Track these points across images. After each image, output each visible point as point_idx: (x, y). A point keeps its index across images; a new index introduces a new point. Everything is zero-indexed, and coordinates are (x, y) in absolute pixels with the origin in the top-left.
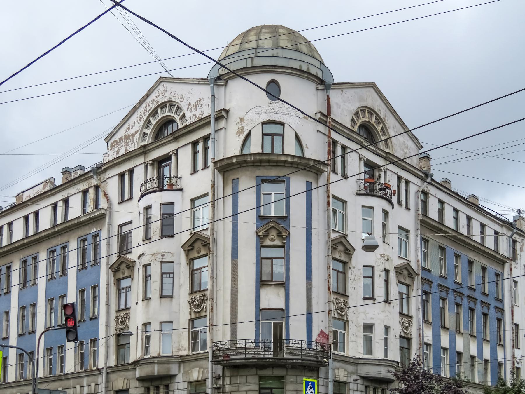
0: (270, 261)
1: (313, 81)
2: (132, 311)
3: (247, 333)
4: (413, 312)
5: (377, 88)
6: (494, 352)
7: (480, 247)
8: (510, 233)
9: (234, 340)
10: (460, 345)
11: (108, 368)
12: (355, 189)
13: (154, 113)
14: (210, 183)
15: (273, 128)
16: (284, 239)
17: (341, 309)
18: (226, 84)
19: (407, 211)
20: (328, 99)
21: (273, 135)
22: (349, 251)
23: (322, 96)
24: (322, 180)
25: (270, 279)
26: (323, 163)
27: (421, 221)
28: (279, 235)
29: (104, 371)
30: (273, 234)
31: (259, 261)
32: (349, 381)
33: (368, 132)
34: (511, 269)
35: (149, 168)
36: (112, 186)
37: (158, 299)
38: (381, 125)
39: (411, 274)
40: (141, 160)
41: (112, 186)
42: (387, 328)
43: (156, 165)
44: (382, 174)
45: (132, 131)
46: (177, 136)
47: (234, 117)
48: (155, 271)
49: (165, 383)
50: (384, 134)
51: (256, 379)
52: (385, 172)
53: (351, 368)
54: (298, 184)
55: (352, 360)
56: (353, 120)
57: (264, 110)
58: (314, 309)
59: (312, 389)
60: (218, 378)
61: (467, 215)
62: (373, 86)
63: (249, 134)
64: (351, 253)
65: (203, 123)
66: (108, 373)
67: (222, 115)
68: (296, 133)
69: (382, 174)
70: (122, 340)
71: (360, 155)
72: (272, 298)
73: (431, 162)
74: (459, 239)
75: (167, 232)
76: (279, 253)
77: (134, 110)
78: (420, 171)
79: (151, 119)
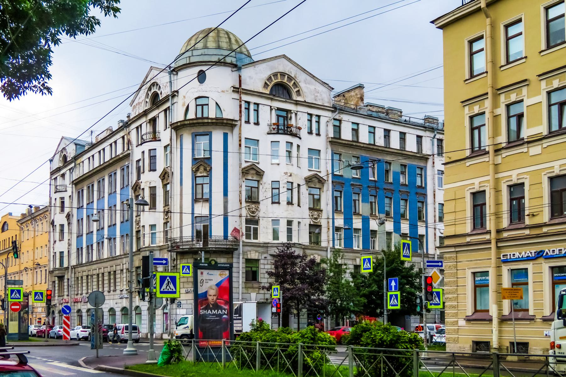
0: (201, 186)
1: (229, 66)
3: (188, 233)
5: (287, 57)
6: (413, 227)
8: (432, 135)
9: (181, 237)
10: (374, 225)
12: (267, 129)
14: (169, 138)
15: (201, 101)
16: (208, 172)
17: (253, 212)
18: (177, 74)
20: (240, 76)
21: (202, 105)
22: (260, 174)
23: (236, 74)
24: (236, 130)
25: (201, 197)
26: (236, 121)
30: (202, 169)
31: (195, 185)
32: (260, 258)
33: (281, 88)
34: (434, 163)
39: (321, 181)
40: (143, 120)
43: (152, 122)
44: (293, 115)
45: (140, 100)
52: (296, 114)
53: (261, 250)
55: (262, 245)
57: (196, 90)
58: (184, 224)
59: (408, 251)
60: (174, 260)
62: (284, 56)
63: (188, 105)
68: (216, 103)
69: (293, 115)
71: (271, 107)
72: (202, 209)
73: (365, 90)
75: (153, 169)
76: (207, 180)
78: (332, 108)
79: (149, 92)
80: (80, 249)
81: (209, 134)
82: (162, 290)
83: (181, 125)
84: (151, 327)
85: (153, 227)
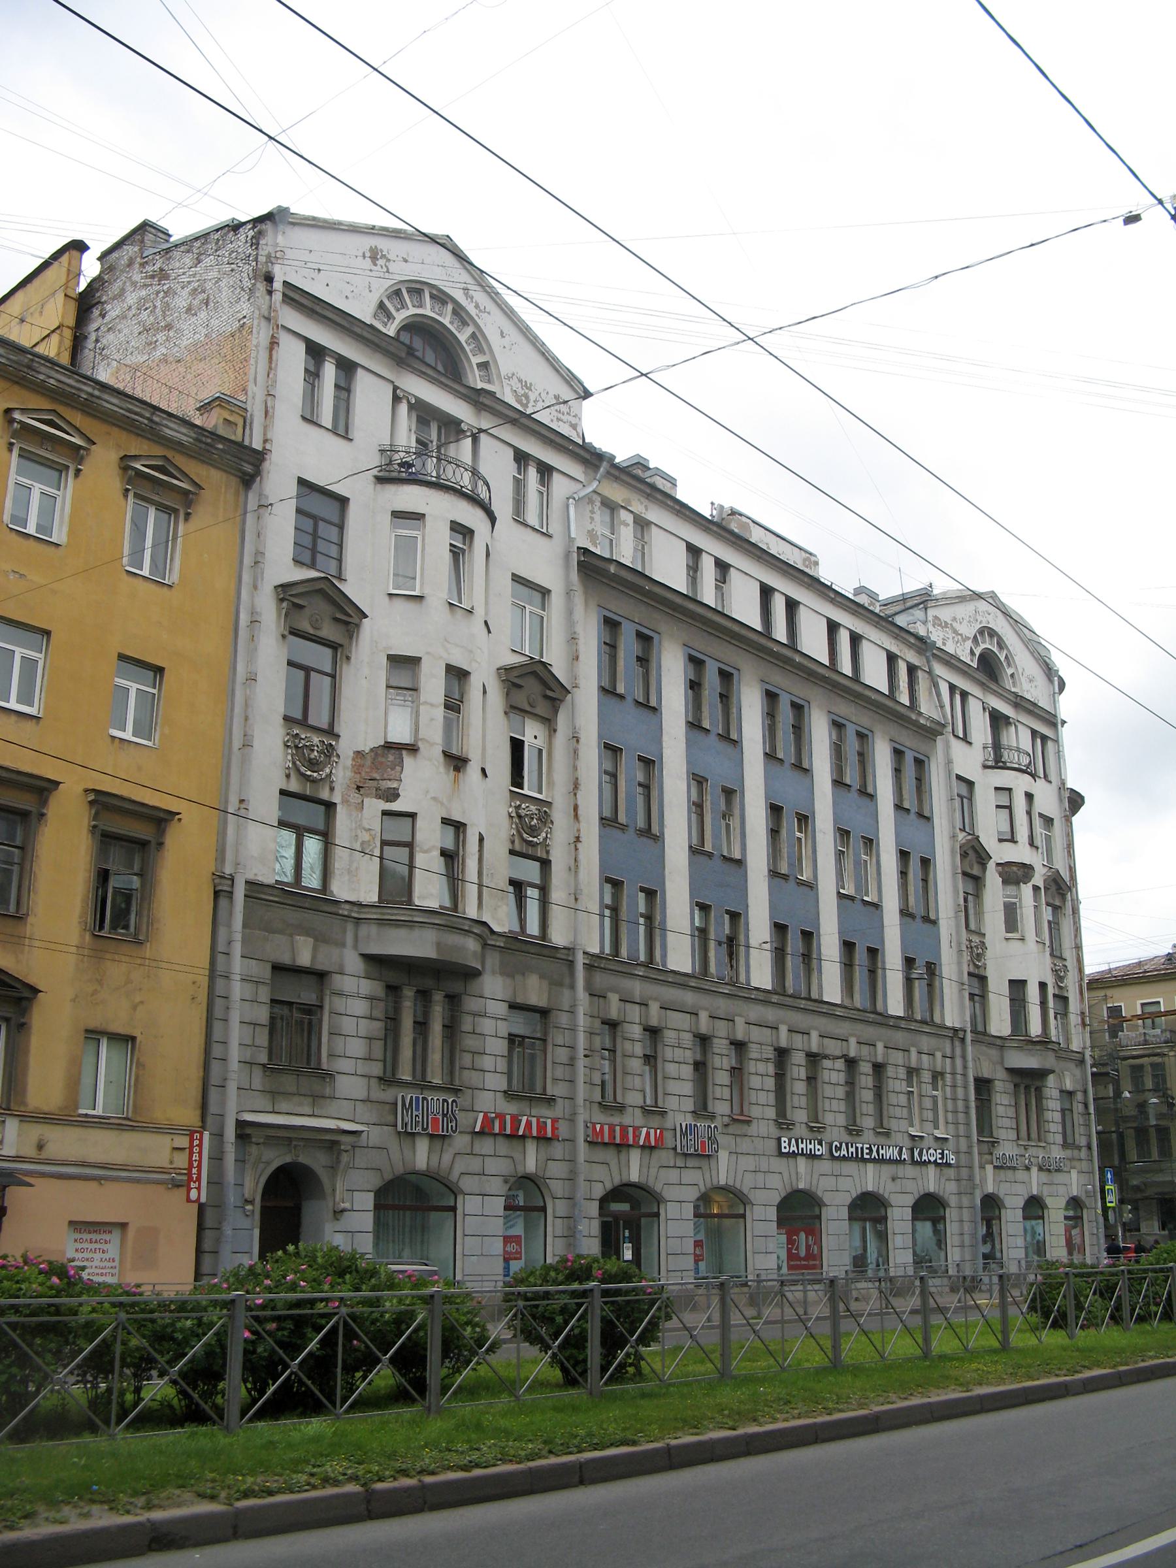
7: (827, 673)
12: (980, 759)
19: (1048, 784)
38: (469, 330)
42: (1043, 986)
50: (481, 350)
56: (381, 306)
61: (887, 650)
64: (355, 620)
71: (395, 388)
74: (771, 653)
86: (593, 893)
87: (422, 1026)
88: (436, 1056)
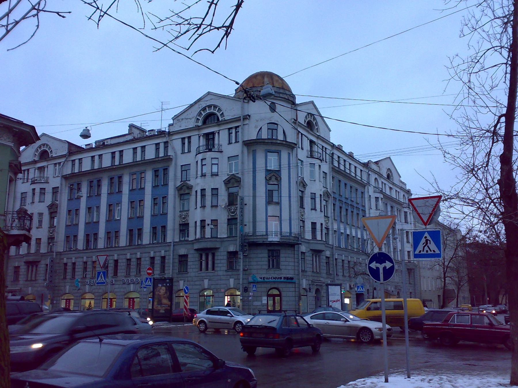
2: (190, 213)
4: (329, 215)
11: (174, 242)
13: (204, 109)
15: (273, 126)
21: (272, 130)
22: (304, 185)
27: (332, 168)
28: (276, 179)
29: (172, 244)
35: (201, 137)
36: (176, 143)
37: (210, 208)
40: (196, 133)
41: (176, 143)
42: (322, 224)
46: (219, 123)
47: (253, 118)
48: (208, 193)
49: (213, 252)
51: (266, 251)
54: (284, 154)
65: (238, 120)
66: (174, 245)
67: (247, 117)
70: (184, 227)
77: (191, 106)
79: (202, 112)
80: (136, 232)
81: (279, 152)
82: (417, 252)
83: (254, 143)
84: (31, 277)
85: (215, 222)
86: (271, 318)
87: (32, 271)
88: (33, 276)
